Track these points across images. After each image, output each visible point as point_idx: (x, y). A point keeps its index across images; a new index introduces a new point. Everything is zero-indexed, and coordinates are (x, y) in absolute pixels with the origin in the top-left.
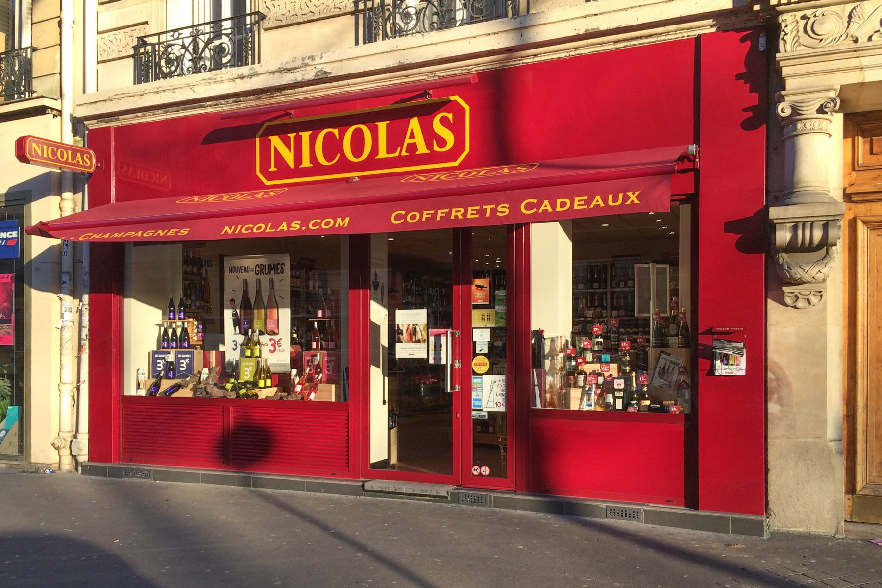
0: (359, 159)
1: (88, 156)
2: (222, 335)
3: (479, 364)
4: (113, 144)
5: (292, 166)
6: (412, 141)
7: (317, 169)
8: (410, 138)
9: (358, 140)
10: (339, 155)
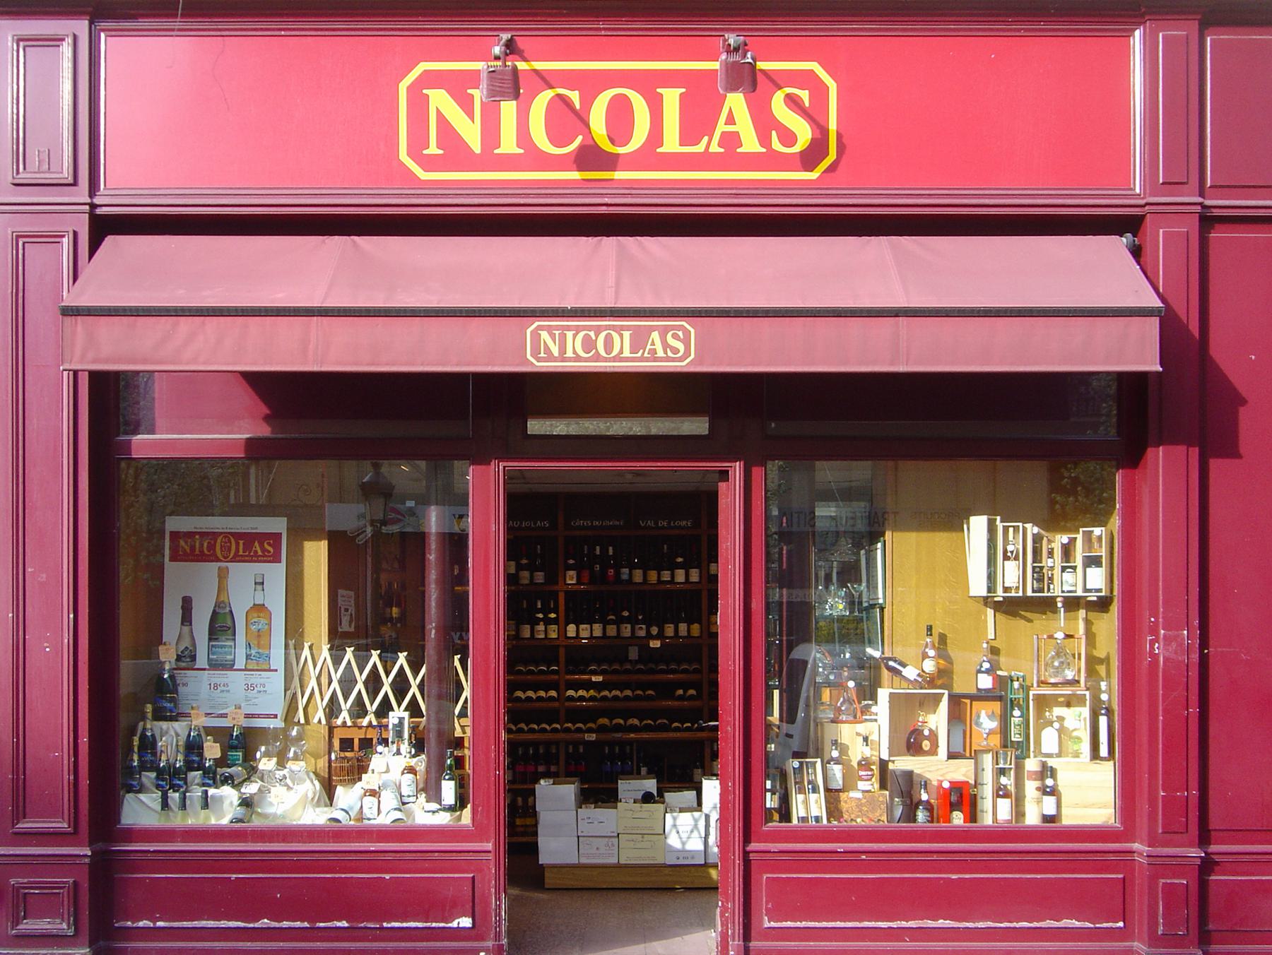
0: (612, 95)
1: (804, 95)
4: (918, 875)
8: (651, 345)
9: (620, 116)
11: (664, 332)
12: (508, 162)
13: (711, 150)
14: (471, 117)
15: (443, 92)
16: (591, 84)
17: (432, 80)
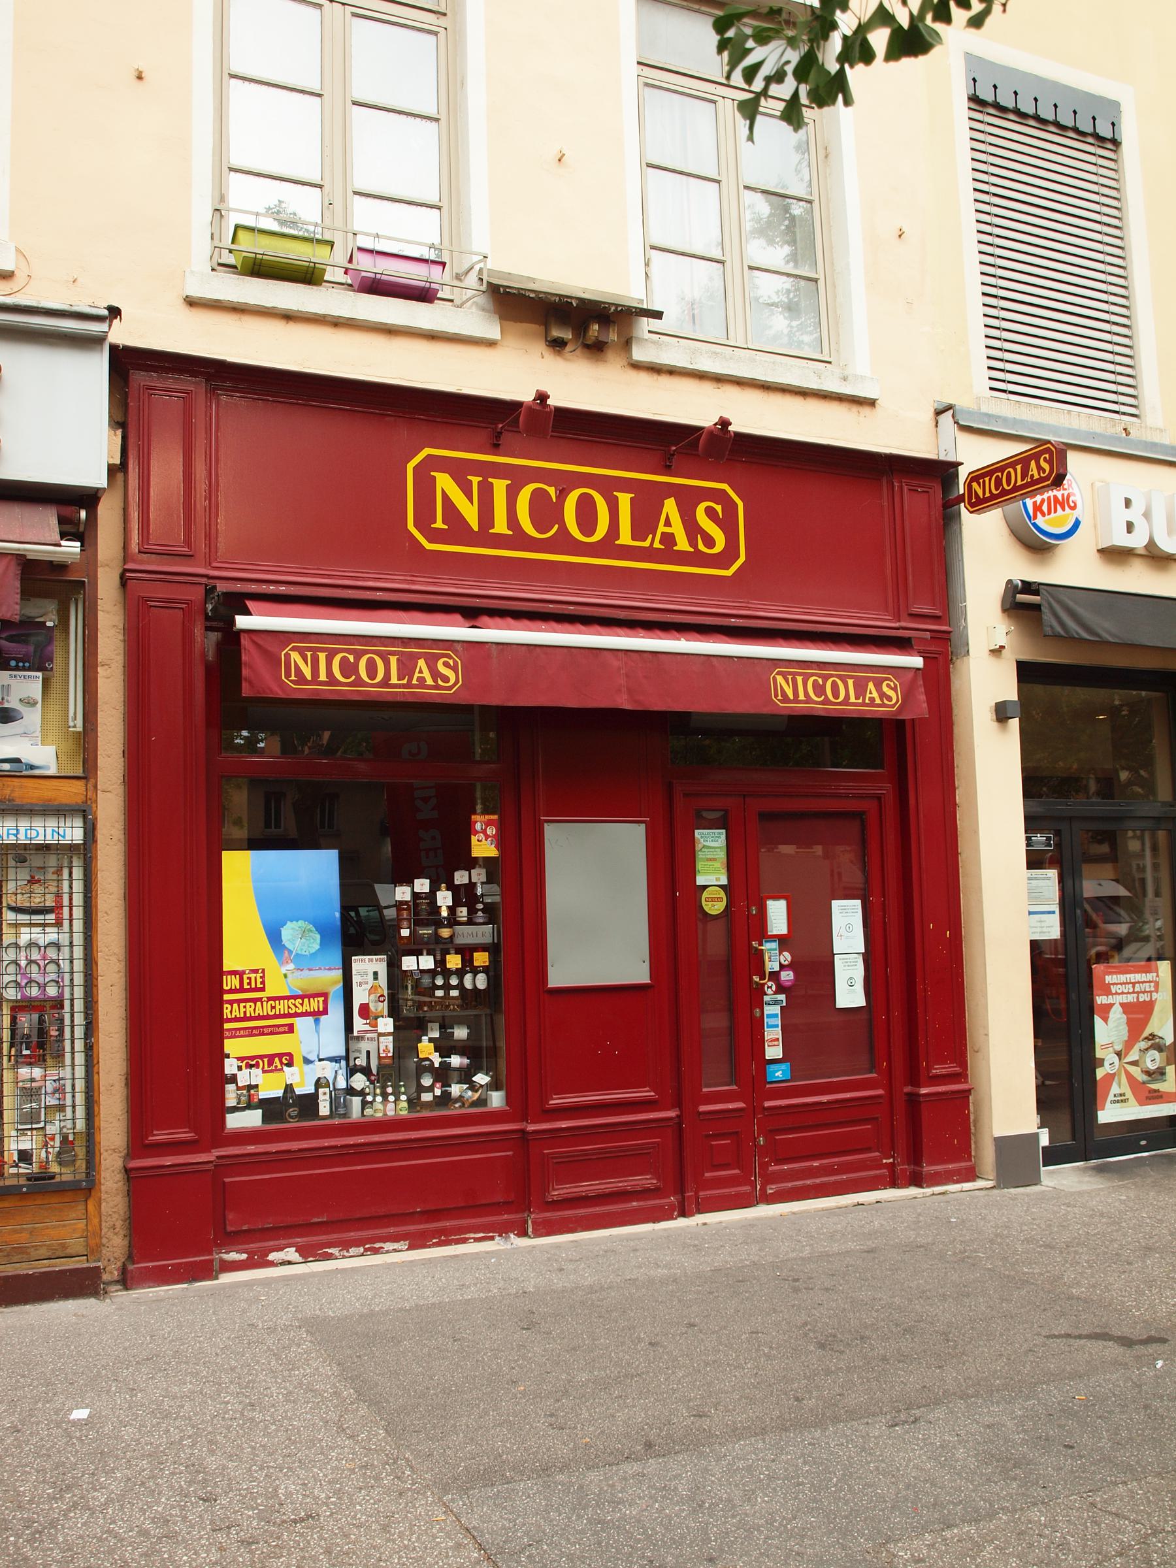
2: (245, 844)
3: (712, 900)
5: (476, 529)
6: (667, 530)
7: (518, 539)
8: (419, 673)
10: (556, 527)
11: (688, 500)
12: (499, 541)
13: (655, 546)
14: (443, 492)
15: (447, 475)
16: (566, 483)
17: (433, 463)
